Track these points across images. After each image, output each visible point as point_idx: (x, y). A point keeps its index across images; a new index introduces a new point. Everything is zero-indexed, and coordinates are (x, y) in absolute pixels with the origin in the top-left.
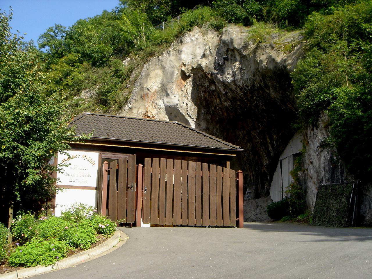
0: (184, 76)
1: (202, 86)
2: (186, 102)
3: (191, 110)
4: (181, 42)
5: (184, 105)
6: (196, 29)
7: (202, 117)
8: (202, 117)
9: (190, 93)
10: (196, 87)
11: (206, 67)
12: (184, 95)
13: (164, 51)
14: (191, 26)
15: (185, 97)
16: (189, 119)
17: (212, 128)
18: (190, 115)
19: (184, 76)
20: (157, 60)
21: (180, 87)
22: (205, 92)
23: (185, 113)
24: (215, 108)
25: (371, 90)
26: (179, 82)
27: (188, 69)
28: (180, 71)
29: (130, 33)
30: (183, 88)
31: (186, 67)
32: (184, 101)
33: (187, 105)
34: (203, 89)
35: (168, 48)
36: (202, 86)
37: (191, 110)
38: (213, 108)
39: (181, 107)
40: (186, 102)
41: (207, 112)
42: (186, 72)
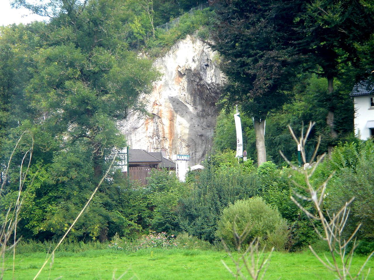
0: (181, 75)
1: (195, 81)
2: (184, 93)
3: (188, 98)
4: (178, 47)
5: (183, 95)
6: (188, 37)
7: (198, 102)
8: (198, 102)
9: (186, 87)
10: (190, 82)
11: (195, 69)
12: (182, 89)
13: (166, 53)
14: (184, 35)
15: (183, 90)
16: (188, 105)
17: (207, 109)
18: (188, 102)
19: (181, 75)
20: (161, 60)
21: (178, 83)
22: (197, 85)
23: (184, 101)
24: (207, 96)
25: (373, 49)
26: (177, 79)
27: (183, 70)
28: (177, 71)
29: (140, 34)
30: (181, 83)
31: (181, 69)
32: (182, 93)
33: (185, 95)
34: (196, 83)
35: (169, 52)
36: (195, 81)
37: (188, 98)
38: (205, 96)
39: (180, 97)
40: (184, 93)
41: (202, 98)
42: (181, 72)
